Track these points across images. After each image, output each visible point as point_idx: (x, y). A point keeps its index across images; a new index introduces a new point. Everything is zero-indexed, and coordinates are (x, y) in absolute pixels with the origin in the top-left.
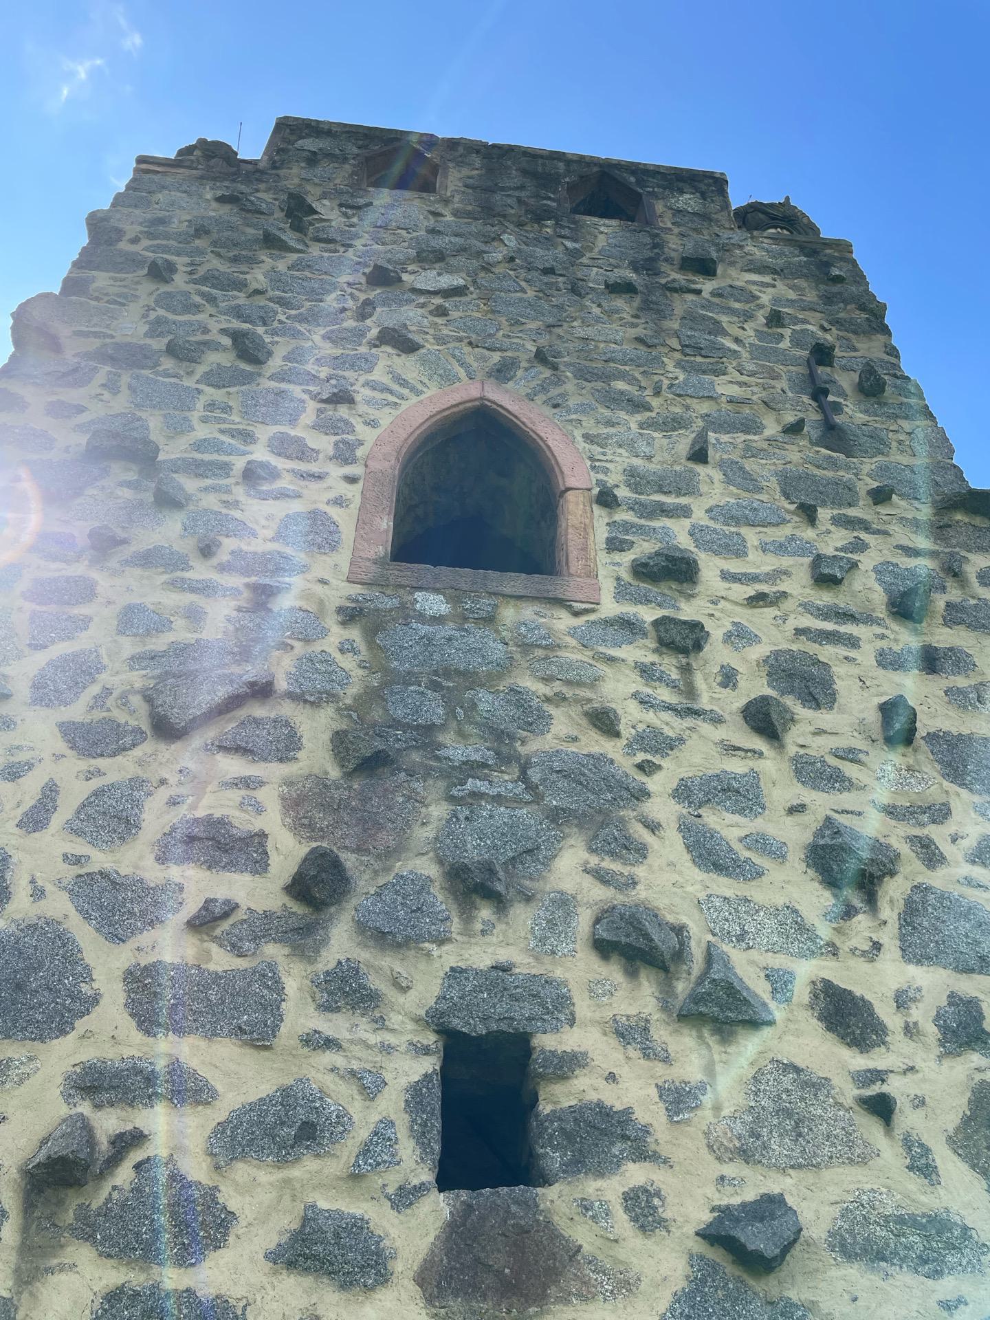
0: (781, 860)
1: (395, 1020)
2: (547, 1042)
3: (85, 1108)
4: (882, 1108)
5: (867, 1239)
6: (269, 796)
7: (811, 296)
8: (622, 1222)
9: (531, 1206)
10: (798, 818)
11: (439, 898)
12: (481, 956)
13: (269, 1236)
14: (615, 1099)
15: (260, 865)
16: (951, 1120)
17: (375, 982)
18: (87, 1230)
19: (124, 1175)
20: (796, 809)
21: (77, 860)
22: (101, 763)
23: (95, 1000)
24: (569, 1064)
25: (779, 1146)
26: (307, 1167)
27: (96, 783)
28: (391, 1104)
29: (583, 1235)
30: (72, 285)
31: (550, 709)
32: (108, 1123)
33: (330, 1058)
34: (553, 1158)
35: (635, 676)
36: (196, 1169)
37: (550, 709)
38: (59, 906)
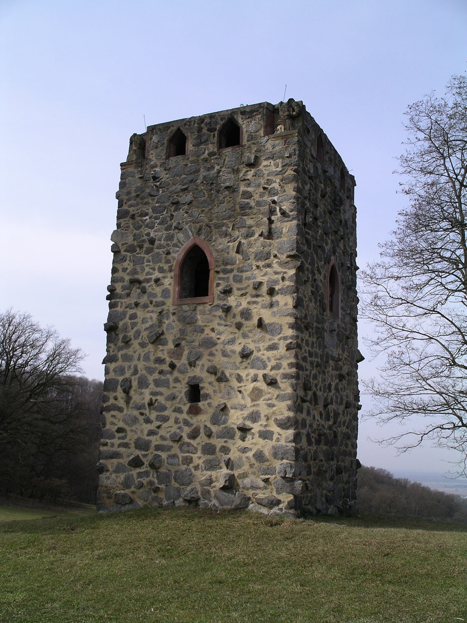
0: (410, 106)
1: (183, 384)
2: (200, 385)
3: (151, 396)
4: (240, 392)
5: (176, 472)
6: (165, 352)
7: (111, 491)
8: (207, 406)
9: (197, 405)
10: (240, 345)
11: (188, 367)
12: (192, 375)
13: (172, 409)
14: (207, 392)
15: (165, 363)
16: (249, 392)
17: (180, 379)
18: (154, 409)
19: (156, 404)
20: (144, 479)
21: (144, 365)
22: (144, 349)
23: (150, 384)
24: (203, 388)
25: (226, 397)
26: (174, 402)
27: (144, 353)
28: (183, 394)
29: (202, 408)
30: (118, 225)
31: (204, 328)
32: (154, 398)
33: (176, 389)
34: (201, 399)
35: (218, 319)
36: (163, 402)
37: (204, 328)
38: (144, 372)
